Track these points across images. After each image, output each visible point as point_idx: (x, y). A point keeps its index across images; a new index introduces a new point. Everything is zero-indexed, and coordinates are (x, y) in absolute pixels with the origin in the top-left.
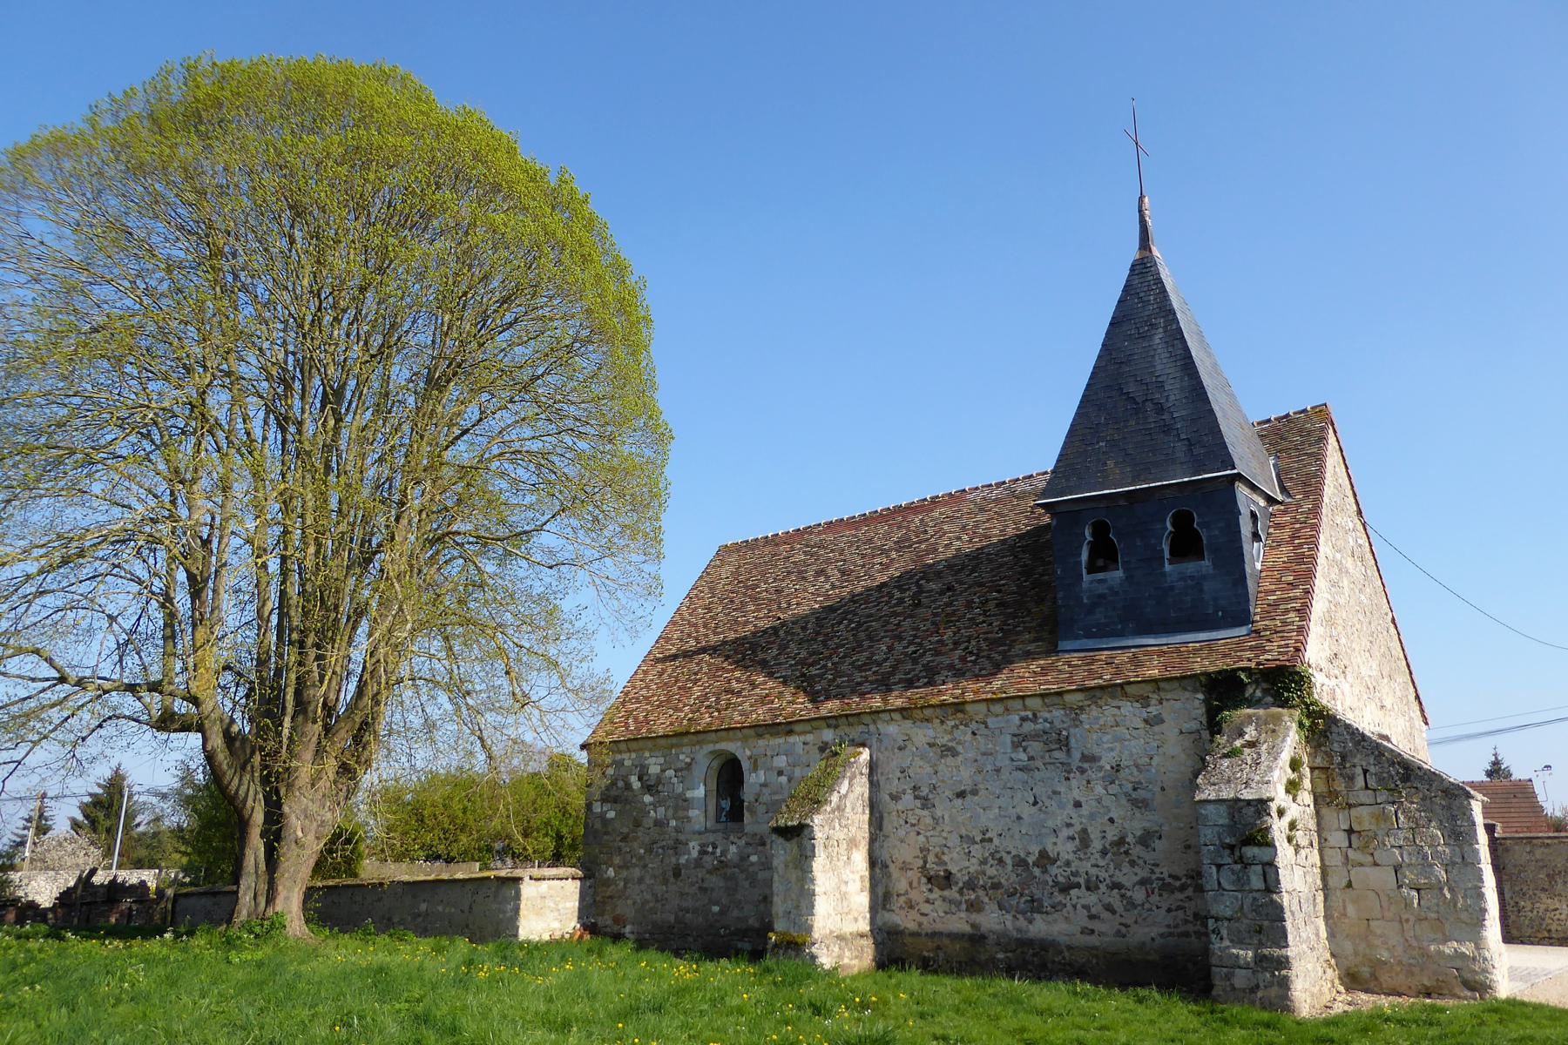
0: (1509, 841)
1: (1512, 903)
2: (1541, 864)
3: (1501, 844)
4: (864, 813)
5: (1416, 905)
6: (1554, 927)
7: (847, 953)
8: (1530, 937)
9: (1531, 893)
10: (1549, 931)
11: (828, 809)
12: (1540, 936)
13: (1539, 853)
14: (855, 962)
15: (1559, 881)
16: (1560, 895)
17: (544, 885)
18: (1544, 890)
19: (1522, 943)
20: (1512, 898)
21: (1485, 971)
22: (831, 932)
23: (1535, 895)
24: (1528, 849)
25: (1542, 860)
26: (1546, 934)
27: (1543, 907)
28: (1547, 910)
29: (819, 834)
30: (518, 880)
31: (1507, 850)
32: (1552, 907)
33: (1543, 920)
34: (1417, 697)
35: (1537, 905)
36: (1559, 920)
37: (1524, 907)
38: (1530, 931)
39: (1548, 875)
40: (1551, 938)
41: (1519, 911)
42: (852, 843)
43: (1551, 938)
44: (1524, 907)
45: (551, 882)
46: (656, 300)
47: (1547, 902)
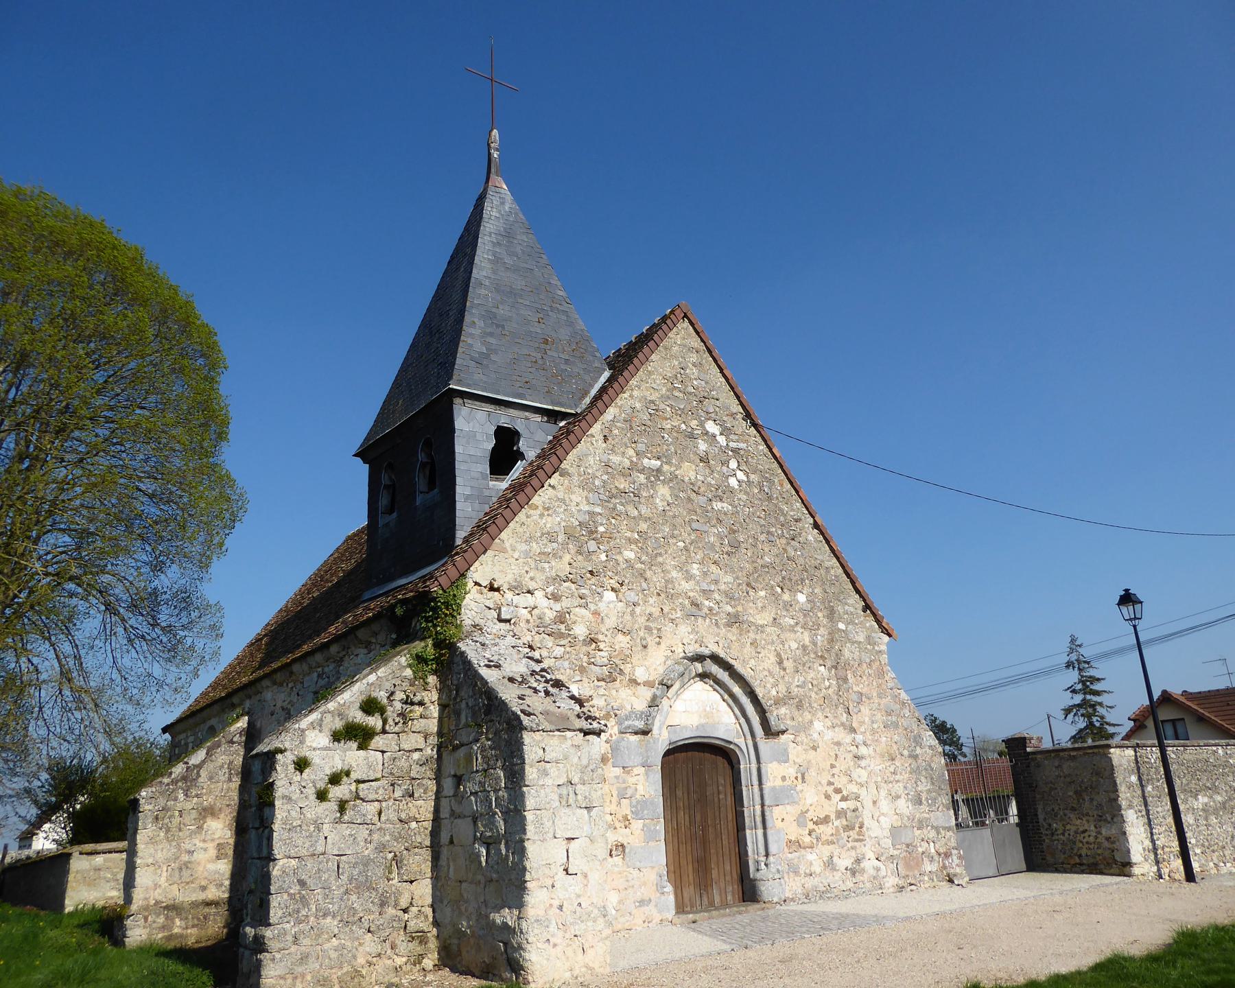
0: (1039, 756)
1: (1046, 826)
2: (1068, 780)
3: (1032, 759)
4: (230, 780)
5: (484, 864)
6: (1084, 852)
7: (178, 922)
8: (1063, 863)
9: (1061, 813)
10: (1080, 856)
11: (166, 780)
12: (1072, 862)
13: (1067, 767)
14: (193, 931)
15: (1087, 798)
16: (1088, 814)
17: (99, 859)
18: (1073, 809)
19: (1057, 871)
20: (1045, 820)
21: (520, 947)
22: (157, 903)
23: (1065, 815)
24: (1057, 764)
25: (1070, 775)
26: (1078, 860)
27: (1073, 828)
28: (1076, 832)
29: (146, 807)
30: (69, 855)
31: (1038, 766)
32: (1081, 829)
33: (1074, 843)
34: (867, 607)
35: (1068, 827)
36: (1087, 843)
37: (1056, 830)
38: (1063, 856)
39: (1076, 792)
40: (1081, 864)
41: (1053, 834)
42: (208, 812)
43: (1081, 864)
44: (1056, 830)
45: (108, 855)
46: (228, 345)
47: (1077, 823)
